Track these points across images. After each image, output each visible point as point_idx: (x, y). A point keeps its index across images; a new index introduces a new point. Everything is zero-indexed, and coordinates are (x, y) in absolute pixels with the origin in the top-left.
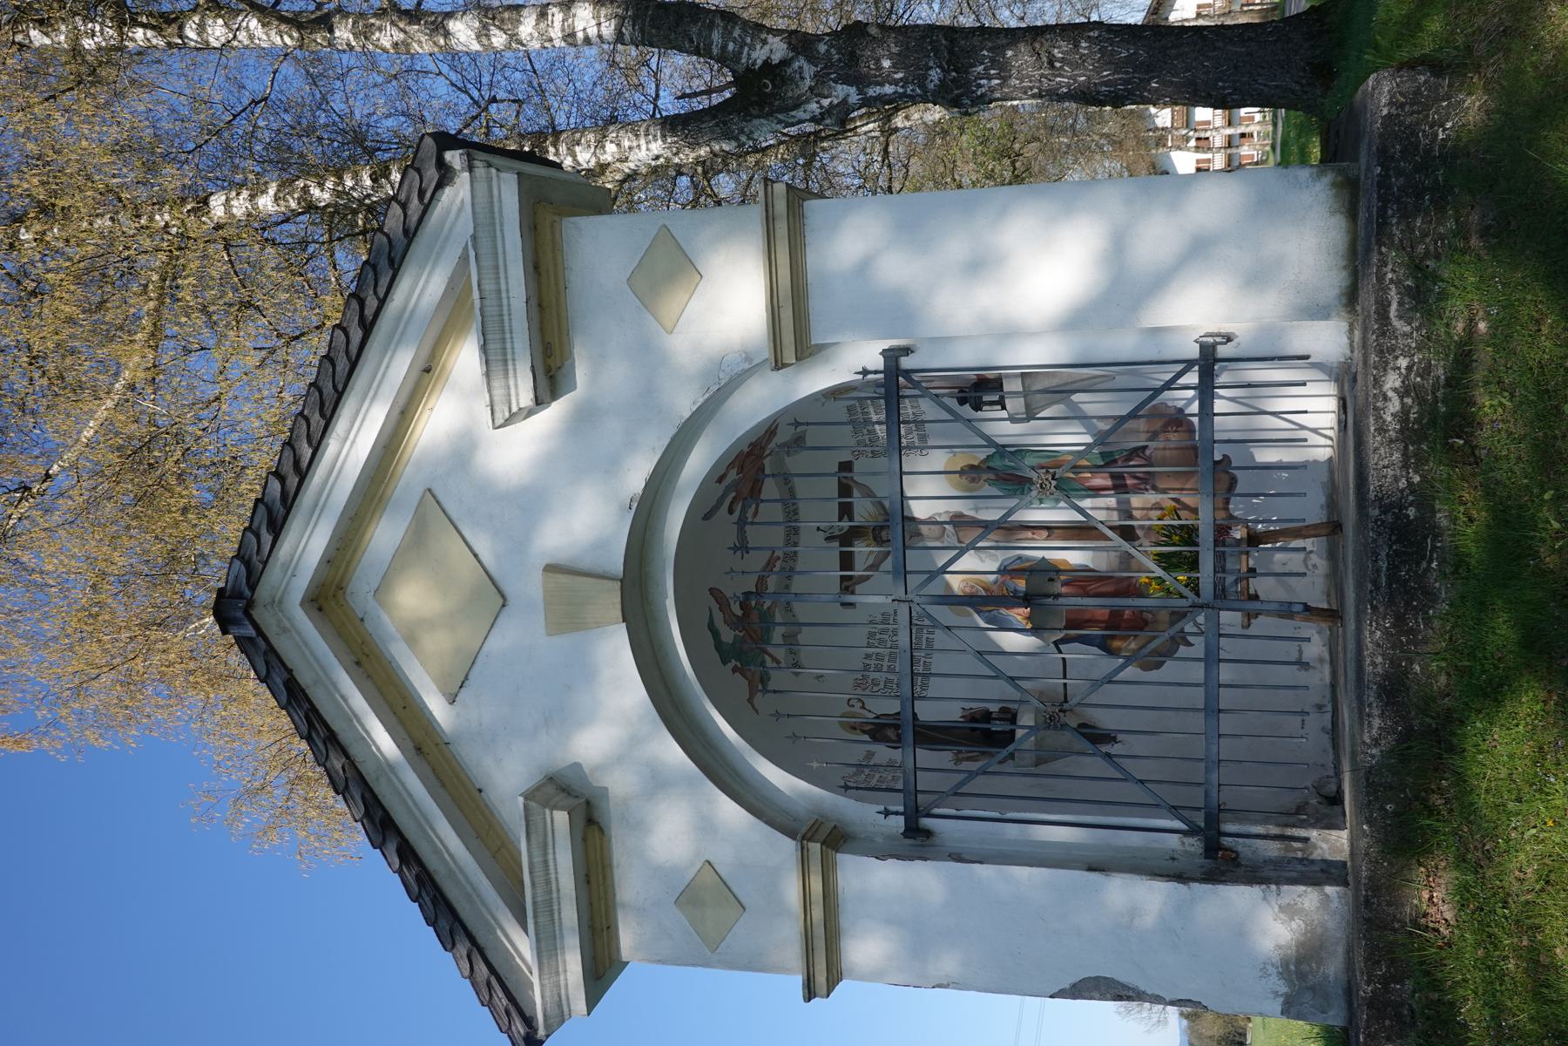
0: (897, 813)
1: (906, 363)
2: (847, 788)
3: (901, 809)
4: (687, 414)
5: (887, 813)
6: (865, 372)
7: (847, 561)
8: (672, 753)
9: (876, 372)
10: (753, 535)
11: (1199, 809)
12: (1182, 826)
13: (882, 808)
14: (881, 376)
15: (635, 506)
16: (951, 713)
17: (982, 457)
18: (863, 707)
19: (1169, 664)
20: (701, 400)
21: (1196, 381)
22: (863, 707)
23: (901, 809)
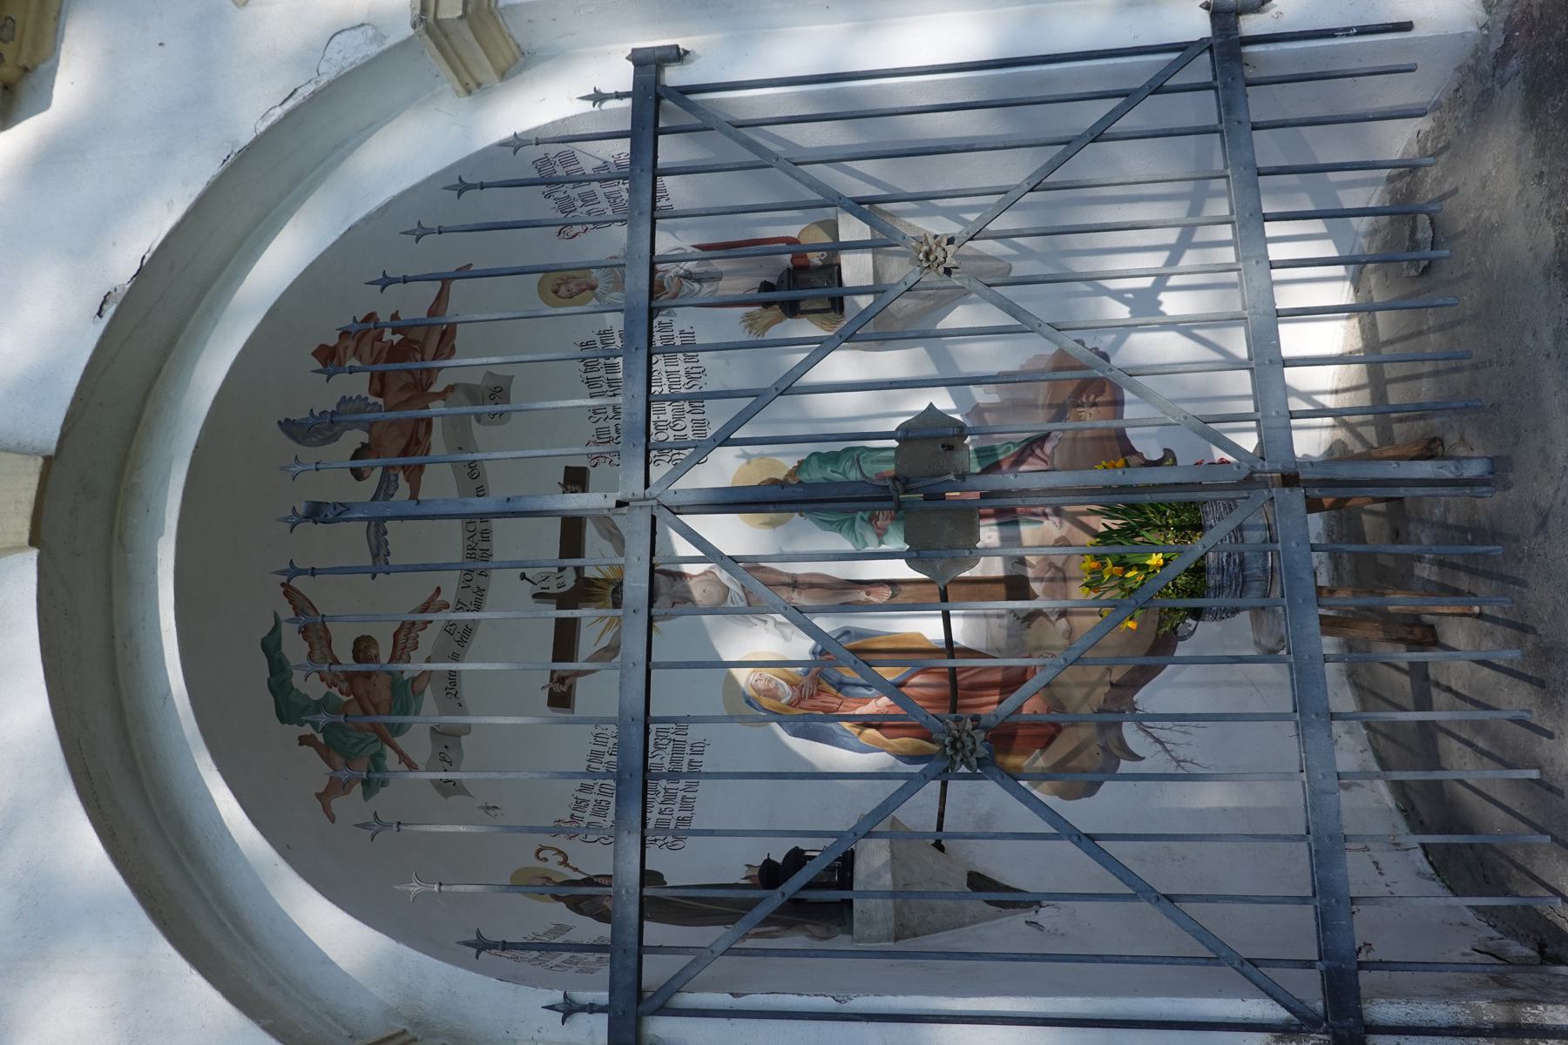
0: (591, 1008)
1: (674, 76)
2: (481, 945)
3: (602, 997)
4: (246, 138)
5: (569, 1009)
6: (598, 97)
7: (565, 640)
8: (81, 847)
9: (618, 96)
10: (404, 540)
11: (1308, 964)
12: (1278, 1013)
13: (557, 997)
14: (628, 102)
15: (110, 310)
16: (730, 863)
17: (790, 463)
18: (565, 862)
19: (1107, 786)
20: (278, 112)
21: (1207, 77)
22: (565, 862)
23: (602, 997)
